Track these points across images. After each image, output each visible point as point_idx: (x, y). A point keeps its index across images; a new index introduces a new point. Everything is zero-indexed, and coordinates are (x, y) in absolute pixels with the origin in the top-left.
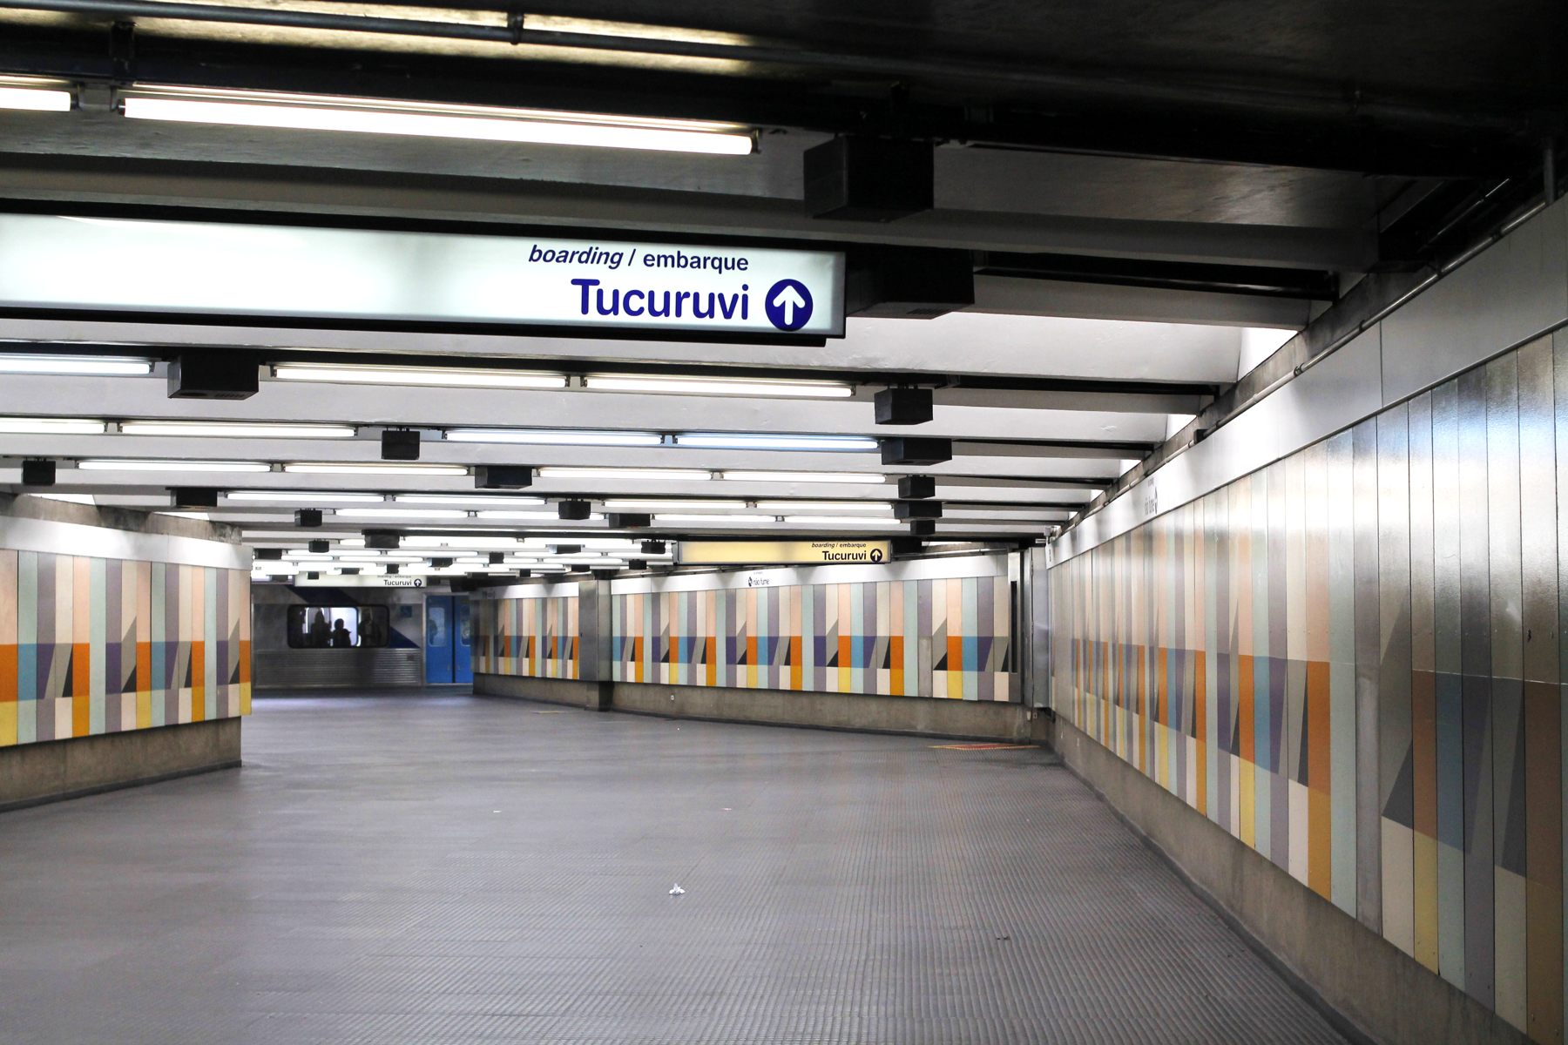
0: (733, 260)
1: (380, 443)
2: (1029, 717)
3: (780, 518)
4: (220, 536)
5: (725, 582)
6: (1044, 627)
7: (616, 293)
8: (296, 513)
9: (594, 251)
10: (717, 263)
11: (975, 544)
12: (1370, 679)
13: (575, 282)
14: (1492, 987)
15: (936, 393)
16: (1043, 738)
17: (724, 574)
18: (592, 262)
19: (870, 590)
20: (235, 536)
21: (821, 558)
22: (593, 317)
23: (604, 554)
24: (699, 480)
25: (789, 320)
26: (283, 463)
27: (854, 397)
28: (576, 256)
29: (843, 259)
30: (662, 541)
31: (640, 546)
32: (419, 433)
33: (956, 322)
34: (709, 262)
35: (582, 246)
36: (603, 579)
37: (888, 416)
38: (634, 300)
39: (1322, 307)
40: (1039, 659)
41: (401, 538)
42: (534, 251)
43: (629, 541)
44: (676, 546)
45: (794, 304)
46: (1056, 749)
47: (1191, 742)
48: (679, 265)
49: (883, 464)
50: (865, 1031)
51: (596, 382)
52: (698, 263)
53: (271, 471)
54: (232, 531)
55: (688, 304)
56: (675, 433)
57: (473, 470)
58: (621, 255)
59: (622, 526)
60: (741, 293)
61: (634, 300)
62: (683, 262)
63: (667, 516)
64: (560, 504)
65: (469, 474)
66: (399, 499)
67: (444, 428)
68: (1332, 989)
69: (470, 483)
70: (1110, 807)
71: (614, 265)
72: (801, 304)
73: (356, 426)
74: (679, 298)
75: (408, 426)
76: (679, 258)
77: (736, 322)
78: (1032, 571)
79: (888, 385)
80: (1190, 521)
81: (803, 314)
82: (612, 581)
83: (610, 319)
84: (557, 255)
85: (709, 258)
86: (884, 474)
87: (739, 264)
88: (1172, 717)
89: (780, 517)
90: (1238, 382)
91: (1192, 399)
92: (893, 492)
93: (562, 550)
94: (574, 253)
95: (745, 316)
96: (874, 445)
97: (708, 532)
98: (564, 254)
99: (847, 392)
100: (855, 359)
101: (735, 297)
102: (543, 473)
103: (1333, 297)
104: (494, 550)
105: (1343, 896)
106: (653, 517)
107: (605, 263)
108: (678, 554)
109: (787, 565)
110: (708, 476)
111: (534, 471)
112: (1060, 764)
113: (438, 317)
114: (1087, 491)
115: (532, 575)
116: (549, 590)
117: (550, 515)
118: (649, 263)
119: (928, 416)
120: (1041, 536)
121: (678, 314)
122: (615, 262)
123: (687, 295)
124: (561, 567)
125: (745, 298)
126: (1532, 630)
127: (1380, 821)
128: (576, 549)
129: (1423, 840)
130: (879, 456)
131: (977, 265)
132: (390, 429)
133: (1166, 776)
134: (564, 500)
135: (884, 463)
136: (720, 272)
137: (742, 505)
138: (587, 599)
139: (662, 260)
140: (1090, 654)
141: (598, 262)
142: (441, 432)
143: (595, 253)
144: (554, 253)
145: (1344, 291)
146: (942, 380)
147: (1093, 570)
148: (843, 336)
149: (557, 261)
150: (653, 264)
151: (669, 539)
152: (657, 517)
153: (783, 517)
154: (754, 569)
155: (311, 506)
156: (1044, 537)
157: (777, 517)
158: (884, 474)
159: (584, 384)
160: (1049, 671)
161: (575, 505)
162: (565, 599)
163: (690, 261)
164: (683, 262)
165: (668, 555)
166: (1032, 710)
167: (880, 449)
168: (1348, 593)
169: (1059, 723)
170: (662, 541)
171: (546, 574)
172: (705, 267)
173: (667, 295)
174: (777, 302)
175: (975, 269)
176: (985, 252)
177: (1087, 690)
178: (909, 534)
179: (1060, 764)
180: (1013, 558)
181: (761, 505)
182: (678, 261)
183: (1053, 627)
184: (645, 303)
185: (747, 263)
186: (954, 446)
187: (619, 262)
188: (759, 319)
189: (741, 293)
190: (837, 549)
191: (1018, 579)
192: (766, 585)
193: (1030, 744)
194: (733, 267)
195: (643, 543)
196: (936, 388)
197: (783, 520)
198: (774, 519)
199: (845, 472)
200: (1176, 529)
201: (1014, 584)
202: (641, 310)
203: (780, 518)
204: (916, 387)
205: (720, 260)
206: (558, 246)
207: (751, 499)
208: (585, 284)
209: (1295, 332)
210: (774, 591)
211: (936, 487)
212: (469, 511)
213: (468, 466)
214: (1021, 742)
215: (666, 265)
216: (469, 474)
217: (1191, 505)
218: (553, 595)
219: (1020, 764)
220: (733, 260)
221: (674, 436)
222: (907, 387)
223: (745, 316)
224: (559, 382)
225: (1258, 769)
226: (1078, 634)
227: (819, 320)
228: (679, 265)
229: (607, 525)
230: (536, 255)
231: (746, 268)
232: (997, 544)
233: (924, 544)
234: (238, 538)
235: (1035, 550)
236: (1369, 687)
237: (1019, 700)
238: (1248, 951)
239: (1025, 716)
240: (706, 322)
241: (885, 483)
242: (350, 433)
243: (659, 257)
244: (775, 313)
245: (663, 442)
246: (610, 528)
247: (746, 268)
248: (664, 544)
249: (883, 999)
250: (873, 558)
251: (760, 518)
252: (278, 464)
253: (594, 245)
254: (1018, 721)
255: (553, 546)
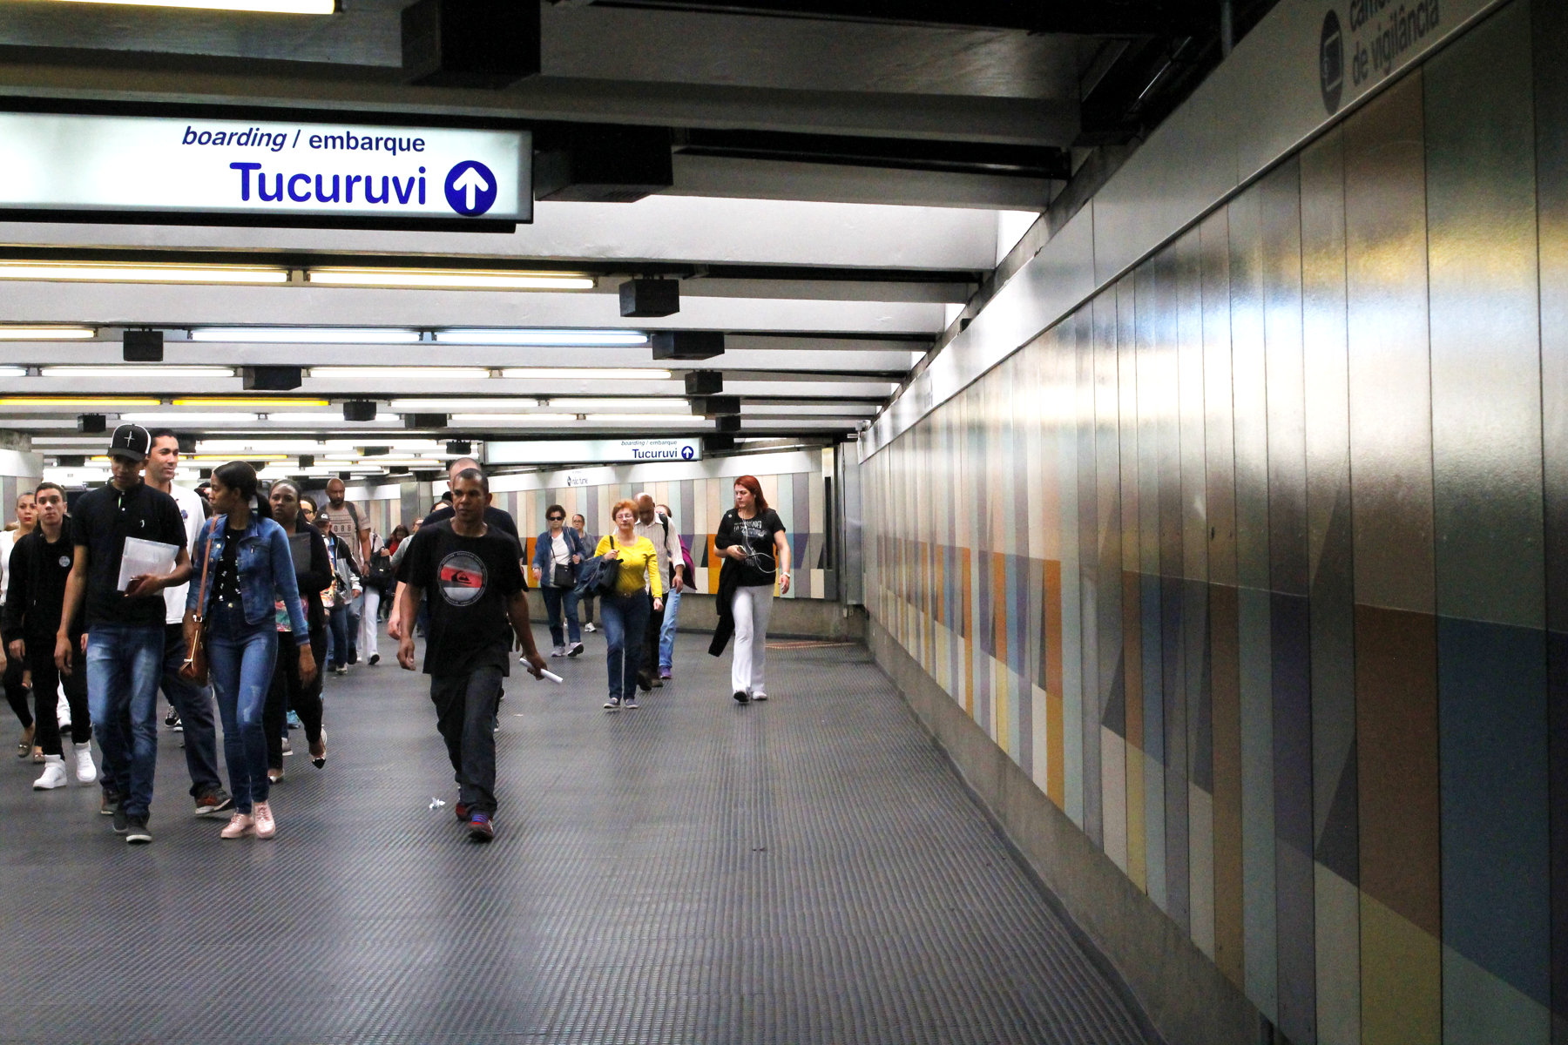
0: (409, 140)
1: (122, 344)
2: (845, 615)
3: (581, 416)
4: (7, 443)
5: (544, 482)
6: (856, 522)
7: (279, 178)
8: (79, 418)
9: (254, 132)
10: (390, 144)
11: (792, 440)
12: (1091, 579)
13: (234, 166)
14: (1187, 911)
15: (683, 284)
16: (859, 634)
17: (543, 474)
18: (253, 144)
19: (687, 487)
20: (23, 443)
21: (631, 457)
22: (255, 204)
23: (418, 455)
24: (476, 378)
25: (471, 204)
26: (39, 367)
27: (597, 289)
28: (235, 139)
29: (529, 139)
30: (467, 441)
31: (445, 447)
32: (162, 333)
33: (655, 204)
34: (381, 143)
35: (241, 127)
36: (425, 480)
37: (632, 308)
38: (300, 184)
39: (1059, 186)
40: (852, 555)
41: (198, 442)
42: (188, 133)
43: (434, 442)
44: (482, 446)
45: (476, 187)
46: (870, 647)
47: (961, 641)
48: (348, 147)
49: (655, 358)
50: (585, 955)
51: (319, 276)
52: (369, 144)
53: (27, 375)
54: (20, 437)
55: (359, 188)
56: (434, 330)
57: (240, 371)
58: (284, 137)
59: (418, 426)
60: (417, 176)
61: (300, 184)
62: (353, 143)
63: (464, 415)
64: (345, 405)
65: (236, 375)
66: (176, 402)
67: (189, 327)
68: (1074, 900)
69: (238, 385)
70: (908, 706)
71: (277, 147)
72: (484, 187)
73: (96, 326)
74: (350, 182)
75: (150, 326)
76: (349, 138)
77: (413, 207)
78: (844, 466)
79: (633, 276)
80: (959, 413)
81: (486, 199)
82: (434, 483)
83: (274, 206)
84: (213, 137)
85: (382, 139)
86: (670, 370)
87: (415, 144)
88: (947, 618)
89: (581, 416)
90: (996, 269)
91: (960, 288)
92: (680, 387)
93: (369, 452)
94: (232, 135)
95: (422, 200)
96: (644, 339)
97: (514, 432)
98: (221, 136)
99: (589, 284)
100: (588, 248)
101: (411, 181)
102: (314, 372)
103: (1065, 175)
104: (304, 453)
105: (1073, 809)
106: (451, 417)
107: (267, 145)
108: (485, 454)
109: (605, 464)
110: (487, 374)
111: (304, 372)
112: (872, 662)
113: (96, 206)
114: (887, 384)
115: (352, 478)
116: (372, 493)
117: (335, 417)
118: (315, 144)
119: (674, 308)
120: (853, 431)
121: (349, 199)
122: (278, 143)
123: (358, 179)
124: (379, 469)
125: (422, 181)
126: (1217, 530)
127: (1100, 731)
128: (383, 451)
129: (1134, 752)
130: (650, 350)
131: (677, 144)
132: (132, 330)
133: (944, 678)
134: (349, 401)
135: (656, 357)
136: (394, 154)
137: (533, 403)
138: (407, 498)
139: (330, 141)
140: (895, 550)
141: (259, 145)
142: (186, 332)
143: (256, 135)
144: (210, 134)
145: (1075, 169)
146: (689, 270)
147: (910, 464)
148: (530, 221)
149: (214, 143)
150: (320, 146)
151: (474, 439)
152: (454, 417)
153: (266, 414)
154: (573, 468)
155: (94, 411)
156: (856, 432)
157: (578, 415)
158: (670, 370)
159: (307, 278)
160: (860, 569)
161: (360, 406)
162: (388, 501)
163: (360, 142)
164: (353, 143)
165: (474, 455)
166: (848, 607)
167: (651, 344)
168: (1074, 491)
169: (872, 620)
170: (467, 441)
171: (368, 476)
172: (377, 148)
173: (336, 179)
174: (457, 186)
175: (675, 149)
176: (686, 129)
177: (888, 587)
178: (715, 431)
179: (872, 662)
180: (828, 453)
181: (554, 403)
182: (348, 143)
183: (864, 523)
184: (312, 187)
185: (423, 144)
186: (726, 338)
187: (282, 144)
188: (437, 204)
189: (417, 176)
190: (648, 446)
191: (832, 474)
192: (585, 484)
193: (847, 641)
194: (408, 149)
195: (448, 444)
196: (684, 278)
197: (585, 418)
198: (575, 417)
199: (115, 365)
200: (948, 422)
201: (828, 480)
202: (308, 196)
203: (581, 416)
204: (662, 278)
205: (394, 140)
206: (215, 127)
207: (543, 397)
208: (245, 168)
209: (1037, 214)
210: (593, 492)
211: (724, 382)
212: (259, 414)
213: (235, 367)
214: (837, 640)
215: (334, 147)
216: (236, 375)
217: (957, 398)
218: (376, 498)
219: (834, 662)
220: (409, 140)
221: (433, 333)
222: (653, 277)
223: (422, 200)
224: (280, 276)
225: (1009, 670)
226: (881, 530)
227: (505, 204)
228: (348, 147)
229: (403, 425)
230: (190, 138)
231: (422, 149)
232: (812, 440)
233: (737, 440)
234: (26, 445)
235: (847, 445)
236: (1089, 586)
237: (834, 597)
238: (1009, 861)
239: (841, 612)
240: (379, 208)
241: (672, 379)
242: (90, 334)
243: (326, 138)
244: (456, 198)
245: (421, 339)
246: (406, 429)
247: (422, 149)
248: (470, 444)
249: (704, 896)
250: (684, 455)
251: (558, 415)
252: (34, 368)
253: (254, 125)
254: (835, 618)
255: (359, 449)
